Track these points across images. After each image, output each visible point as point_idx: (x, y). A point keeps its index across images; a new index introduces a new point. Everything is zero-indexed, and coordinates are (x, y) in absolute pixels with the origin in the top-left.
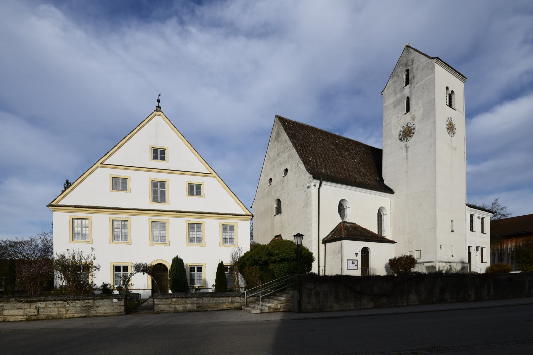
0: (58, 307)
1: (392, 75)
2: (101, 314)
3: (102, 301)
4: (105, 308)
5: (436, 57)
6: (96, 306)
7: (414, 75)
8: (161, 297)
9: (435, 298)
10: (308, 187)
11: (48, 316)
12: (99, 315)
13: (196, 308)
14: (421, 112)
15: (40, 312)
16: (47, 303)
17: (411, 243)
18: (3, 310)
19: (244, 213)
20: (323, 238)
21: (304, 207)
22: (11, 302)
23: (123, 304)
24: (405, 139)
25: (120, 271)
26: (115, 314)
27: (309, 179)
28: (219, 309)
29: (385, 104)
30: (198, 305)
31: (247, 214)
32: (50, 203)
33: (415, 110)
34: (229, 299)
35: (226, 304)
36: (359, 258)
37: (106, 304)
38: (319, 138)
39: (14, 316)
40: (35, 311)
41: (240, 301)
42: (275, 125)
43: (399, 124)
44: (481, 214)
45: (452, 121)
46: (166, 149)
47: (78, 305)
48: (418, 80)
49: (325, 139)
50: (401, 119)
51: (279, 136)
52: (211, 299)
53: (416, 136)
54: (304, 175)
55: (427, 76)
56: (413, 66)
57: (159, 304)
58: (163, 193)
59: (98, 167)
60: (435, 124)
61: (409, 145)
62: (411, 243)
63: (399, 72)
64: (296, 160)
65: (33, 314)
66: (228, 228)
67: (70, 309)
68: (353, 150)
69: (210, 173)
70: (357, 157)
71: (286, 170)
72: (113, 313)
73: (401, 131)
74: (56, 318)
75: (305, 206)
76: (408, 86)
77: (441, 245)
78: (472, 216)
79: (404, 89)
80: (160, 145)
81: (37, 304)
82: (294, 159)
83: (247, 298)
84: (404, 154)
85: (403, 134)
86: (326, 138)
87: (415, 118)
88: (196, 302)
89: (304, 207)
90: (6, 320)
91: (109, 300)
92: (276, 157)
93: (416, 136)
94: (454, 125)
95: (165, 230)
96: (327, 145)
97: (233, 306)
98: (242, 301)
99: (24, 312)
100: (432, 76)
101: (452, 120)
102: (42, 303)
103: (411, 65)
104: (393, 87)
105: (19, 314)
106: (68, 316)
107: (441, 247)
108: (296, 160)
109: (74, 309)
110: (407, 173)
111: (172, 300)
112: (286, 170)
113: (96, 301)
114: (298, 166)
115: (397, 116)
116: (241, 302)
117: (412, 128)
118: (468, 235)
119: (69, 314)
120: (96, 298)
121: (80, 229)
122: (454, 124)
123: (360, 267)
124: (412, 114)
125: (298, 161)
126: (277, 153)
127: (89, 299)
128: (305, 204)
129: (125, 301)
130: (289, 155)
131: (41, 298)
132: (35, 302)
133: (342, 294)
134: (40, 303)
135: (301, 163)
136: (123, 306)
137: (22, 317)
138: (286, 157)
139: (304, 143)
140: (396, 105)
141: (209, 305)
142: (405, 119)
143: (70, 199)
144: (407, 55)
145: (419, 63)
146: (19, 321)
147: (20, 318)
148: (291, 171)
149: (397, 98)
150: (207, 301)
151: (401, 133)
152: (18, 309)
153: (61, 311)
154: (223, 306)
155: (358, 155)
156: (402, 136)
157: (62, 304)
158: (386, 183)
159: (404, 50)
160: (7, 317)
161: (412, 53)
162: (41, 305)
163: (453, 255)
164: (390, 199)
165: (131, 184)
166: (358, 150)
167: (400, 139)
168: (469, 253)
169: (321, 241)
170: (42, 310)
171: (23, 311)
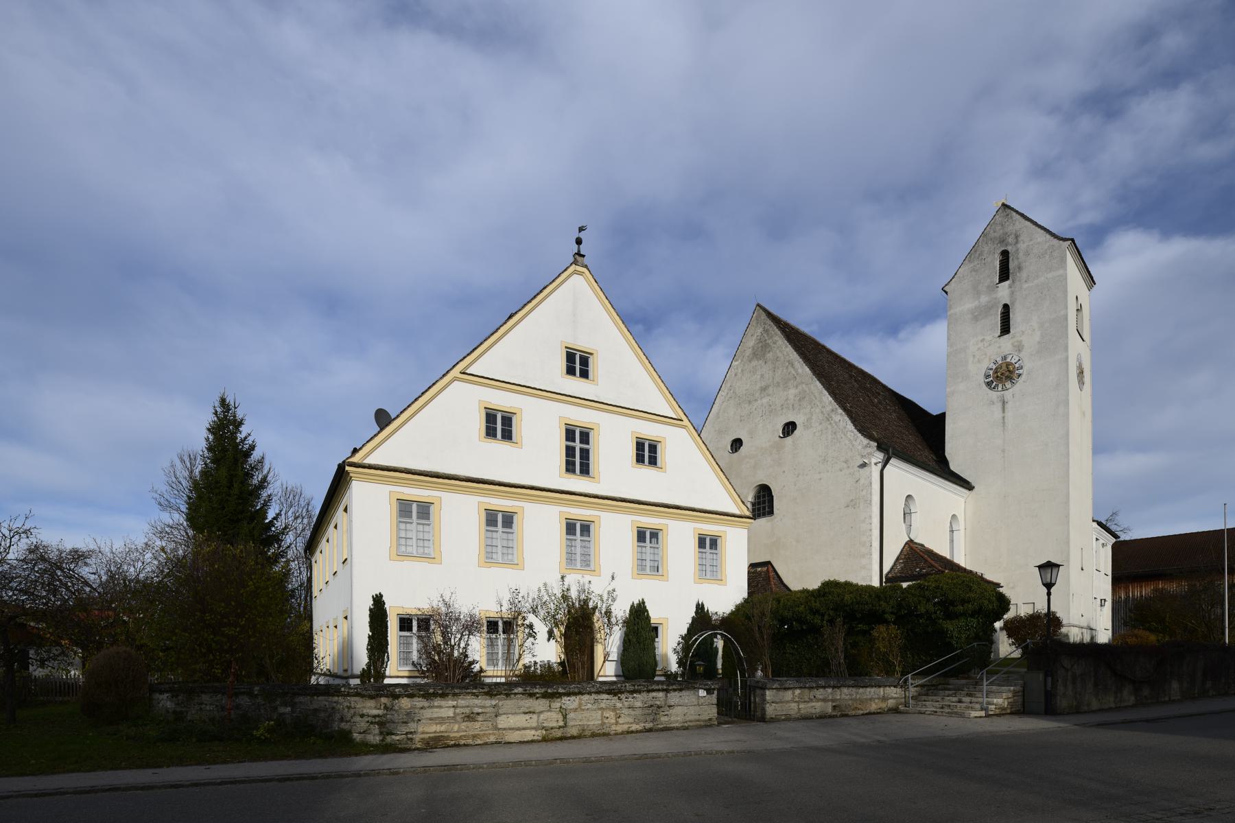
2: (677, 725)
3: (681, 694)
4: (685, 709)
6: (670, 706)
7: (1020, 264)
10: (864, 465)
11: (583, 730)
13: (830, 711)
14: (1037, 336)
15: (568, 721)
17: (1013, 588)
18: (496, 716)
19: (737, 512)
22: (512, 696)
23: (715, 701)
24: (1000, 385)
26: (702, 723)
28: (865, 712)
29: (952, 311)
30: (834, 704)
31: (743, 514)
32: (348, 458)
33: (1023, 332)
35: (876, 701)
39: (519, 729)
40: (560, 717)
41: (895, 696)
42: (754, 323)
43: (986, 354)
46: (591, 354)
47: (638, 704)
48: (1028, 276)
50: (990, 345)
51: (768, 350)
52: (854, 690)
53: (1024, 382)
56: (1019, 246)
58: (585, 454)
60: (1068, 365)
61: (1009, 398)
62: (1013, 588)
63: (986, 252)
64: (823, 407)
65: (555, 724)
66: (707, 543)
67: (623, 711)
69: (676, 417)
71: (790, 428)
72: (698, 721)
75: (852, 504)
76: (1007, 283)
79: (998, 287)
80: (582, 343)
81: (563, 701)
82: (818, 403)
85: (996, 375)
87: (1023, 348)
88: (830, 697)
90: (503, 740)
91: (692, 692)
92: (757, 395)
93: (1024, 382)
95: (513, 533)
100: (1061, 272)
102: (573, 698)
104: (972, 279)
105: (528, 725)
106: (619, 729)
110: (1003, 451)
111: (793, 693)
113: (668, 695)
115: (980, 338)
116: (898, 698)
117: (1017, 365)
120: (671, 688)
121: (421, 530)
124: (1015, 339)
125: (829, 408)
127: (658, 690)
128: (852, 500)
131: (573, 688)
132: (560, 695)
134: (569, 698)
135: (841, 414)
137: (533, 732)
138: (791, 397)
140: (978, 315)
142: (1000, 347)
143: (390, 451)
146: (528, 742)
147: (529, 735)
149: (979, 302)
150: (847, 695)
151: (991, 372)
152: (527, 713)
153: (607, 718)
154: (871, 706)
157: (609, 701)
158: (952, 468)
159: (997, 212)
160: (504, 732)
161: (1015, 221)
162: (570, 702)
164: (963, 500)
165: (521, 427)
167: (989, 384)
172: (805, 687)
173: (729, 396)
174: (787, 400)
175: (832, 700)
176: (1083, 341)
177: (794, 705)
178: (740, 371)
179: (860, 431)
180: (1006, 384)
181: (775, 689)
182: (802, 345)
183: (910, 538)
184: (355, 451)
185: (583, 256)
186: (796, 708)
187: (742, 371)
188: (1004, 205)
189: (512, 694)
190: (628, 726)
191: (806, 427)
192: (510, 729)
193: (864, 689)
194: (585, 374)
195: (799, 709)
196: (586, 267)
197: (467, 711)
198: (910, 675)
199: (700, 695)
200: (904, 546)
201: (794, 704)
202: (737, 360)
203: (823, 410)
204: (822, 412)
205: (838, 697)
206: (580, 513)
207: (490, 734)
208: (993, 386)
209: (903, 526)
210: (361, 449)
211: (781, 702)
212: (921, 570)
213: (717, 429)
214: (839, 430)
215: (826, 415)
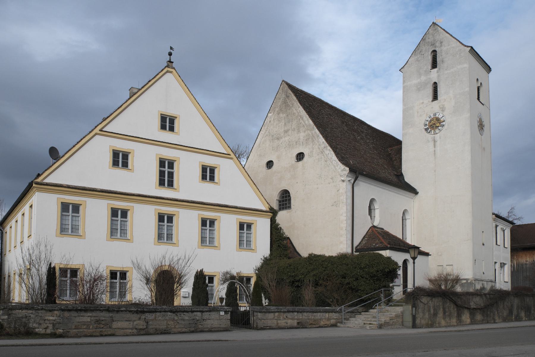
0: (166, 320)
1: (415, 53)
3: (210, 313)
8: (265, 311)
9: (514, 315)
12: (206, 330)
13: (296, 325)
16: (156, 315)
17: (441, 255)
21: (333, 205)
23: (229, 318)
24: (433, 131)
25: (116, 279)
30: (298, 321)
34: (326, 315)
35: (324, 320)
37: (213, 317)
40: (145, 324)
41: (336, 318)
42: (281, 91)
43: (424, 111)
45: (481, 118)
46: (176, 117)
53: (446, 129)
55: (460, 65)
57: (262, 319)
58: (171, 175)
59: (96, 134)
62: (441, 255)
69: (227, 153)
71: (300, 157)
73: (427, 121)
74: (164, 333)
76: (435, 70)
78: (496, 226)
79: (431, 72)
80: (170, 112)
82: (317, 142)
83: (344, 313)
84: (432, 149)
88: (296, 317)
91: (216, 313)
92: (282, 135)
93: (446, 129)
97: (329, 323)
98: (337, 317)
99: (133, 324)
101: (482, 116)
103: (440, 47)
105: (128, 327)
109: (183, 322)
110: (435, 171)
113: (203, 314)
115: (422, 101)
119: (177, 328)
122: (483, 121)
123: (402, 283)
125: (323, 146)
128: (335, 202)
129: (231, 315)
130: (307, 135)
136: (229, 320)
138: (302, 138)
140: (420, 88)
141: (308, 320)
148: (310, 156)
151: (427, 123)
152: (127, 321)
158: (407, 180)
159: (430, 27)
167: (426, 130)
170: (151, 323)
171: (132, 324)
172: (281, 312)
173: (266, 134)
174: (299, 139)
175: (297, 319)
176: (483, 105)
177: (275, 321)
178: (272, 119)
179: (340, 160)
180: (436, 130)
181: (263, 312)
182: (310, 105)
183: (373, 224)
184: (39, 175)
185: (173, 62)
186: (276, 323)
187: (274, 119)
188: (433, 23)
189: (120, 311)
190: (180, 329)
191: (310, 156)
192: (119, 329)
193: (316, 313)
194: (172, 129)
195: (277, 323)
196: (174, 68)
197: (97, 318)
198: (343, 306)
199: (221, 314)
200: (369, 230)
201: (274, 321)
202: (271, 113)
203: (319, 147)
204: (319, 148)
205: (301, 318)
206: (166, 210)
207: (108, 331)
208: (428, 131)
209: (369, 217)
210: (42, 174)
211: (267, 319)
212: (376, 244)
213: (259, 154)
214: (328, 160)
215: (321, 150)
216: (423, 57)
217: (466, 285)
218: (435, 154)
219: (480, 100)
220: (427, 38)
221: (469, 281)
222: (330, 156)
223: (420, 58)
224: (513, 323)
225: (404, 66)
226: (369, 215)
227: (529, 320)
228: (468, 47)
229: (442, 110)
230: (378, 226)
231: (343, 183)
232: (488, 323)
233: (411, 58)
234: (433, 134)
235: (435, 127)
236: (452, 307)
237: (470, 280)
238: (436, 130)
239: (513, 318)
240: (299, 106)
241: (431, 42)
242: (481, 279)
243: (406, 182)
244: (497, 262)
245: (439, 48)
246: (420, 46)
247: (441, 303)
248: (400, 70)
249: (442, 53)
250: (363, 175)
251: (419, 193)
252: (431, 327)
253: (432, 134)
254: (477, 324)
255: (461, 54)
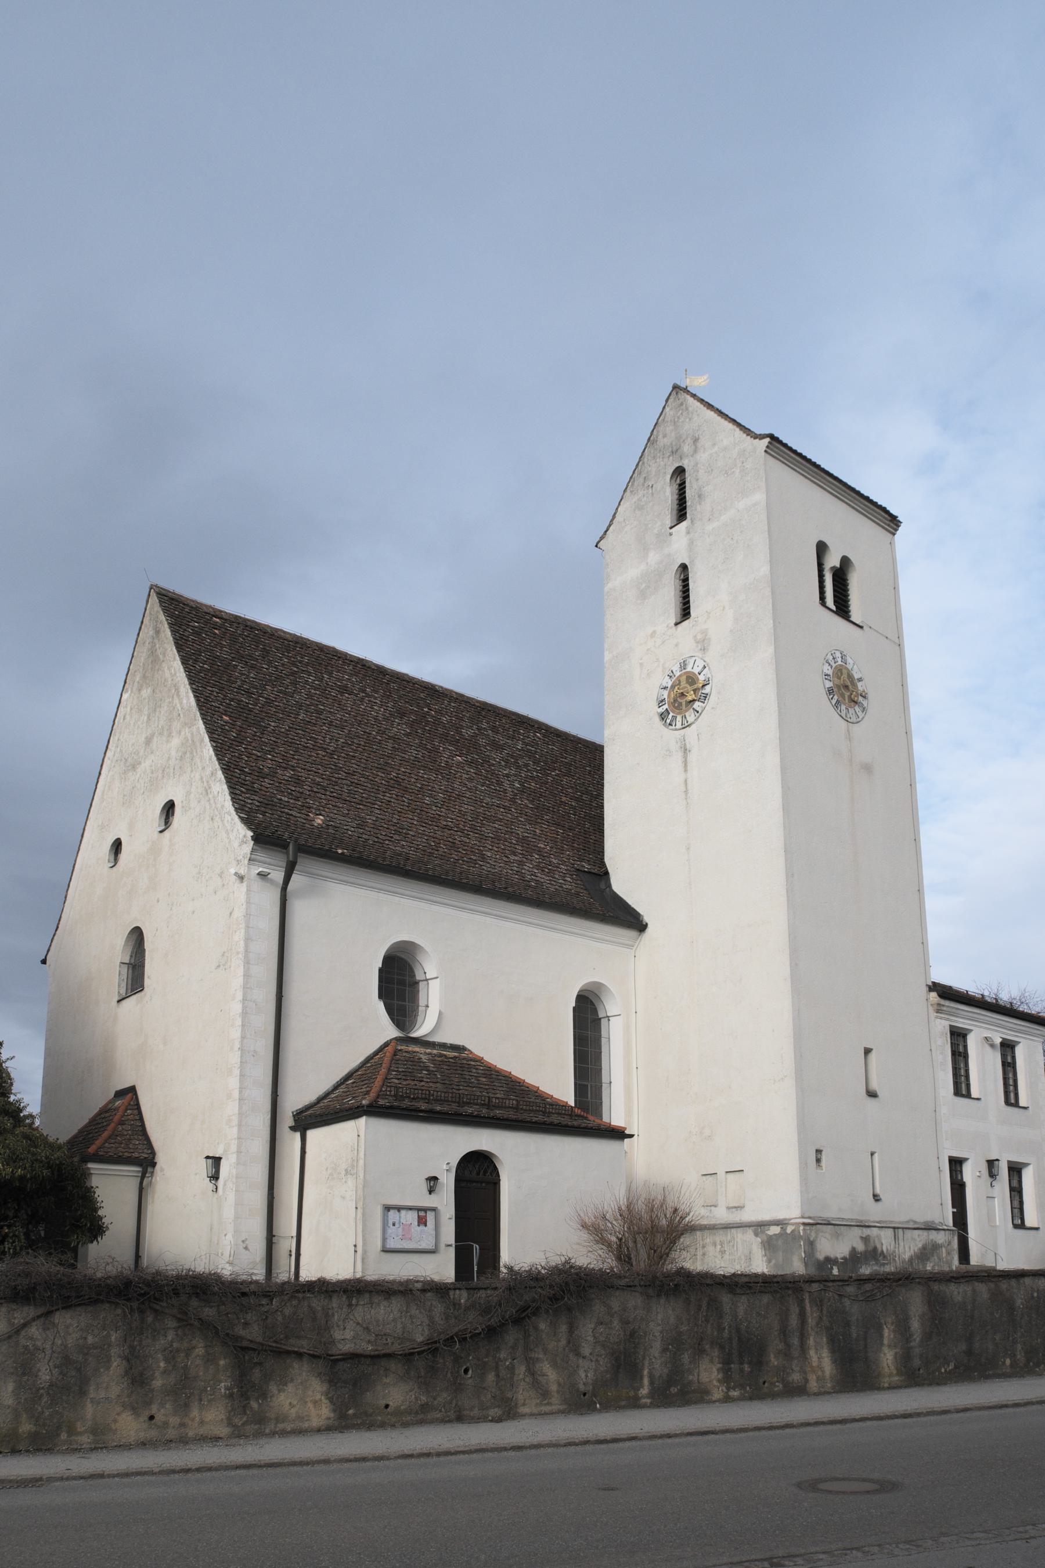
1: (632, 485)
5: (767, 432)
9: (646, 1381)
20: (300, 1105)
21: (219, 966)
24: (679, 718)
27: (240, 845)
33: (708, 613)
36: (445, 1201)
38: (343, 690)
43: (658, 660)
44: (998, 1030)
45: (849, 667)
49: (368, 696)
53: (713, 708)
54: (227, 832)
64: (203, 768)
68: (497, 746)
70: (507, 776)
73: (665, 688)
76: (684, 524)
77: (819, 1152)
78: (958, 1037)
79: (671, 534)
86: (376, 692)
89: (219, 966)
93: (713, 708)
94: (860, 680)
96: (376, 719)
101: (849, 660)
103: (692, 456)
107: (818, 1161)
108: (203, 768)
112: (169, 808)
114: (207, 791)
117: (701, 678)
118: (944, 1110)
122: (856, 676)
123: (451, 1239)
126: (144, 736)
130: (183, 744)
133: (162, 1364)
138: (173, 753)
139: (256, 704)
140: (644, 590)
144: (679, 418)
145: (716, 448)
148: (186, 809)
151: (665, 693)
155: (519, 767)
156: (666, 707)
159: (667, 401)
161: (692, 413)
163: (878, 1191)
166: (519, 750)
167: (663, 716)
168: (958, 1189)
169: (287, 1120)
176: (861, 627)
180: (687, 714)
208: (668, 721)
216: (652, 494)
217: (780, 1242)
218: (686, 792)
219: (852, 619)
220: (660, 436)
221: (789, 1230)
222: (220, 798)
223: (645, 498)
224: (636, 1413)
225: (606, 531)
226: (384, 993)
227: (751, 1399)
228: (761, 437)
229: (701, 650)
230: (431, 1039)
231: (237, 884)
232: (460, 1418)
233: (621, 503)
234: (680, 729)
235: (684, 703)
236: (200, 1351)
237: (792, 1224)
238: (687, 714)
239: (645, 1391)
240: (174, 654)
241: (671, 444)
242: (861, 1222)
243: (615, 893)
244: (875, 1152)
245: (691, 458)
246: (643, 463)
247: (114, 1337)
248: (596, 546)
249: (698, 471)
250: (327, 855)
251: (649, 926)
252: (39, 1450)
253: (677, 727)
254: (370, 1426)
255: (744, 464)
